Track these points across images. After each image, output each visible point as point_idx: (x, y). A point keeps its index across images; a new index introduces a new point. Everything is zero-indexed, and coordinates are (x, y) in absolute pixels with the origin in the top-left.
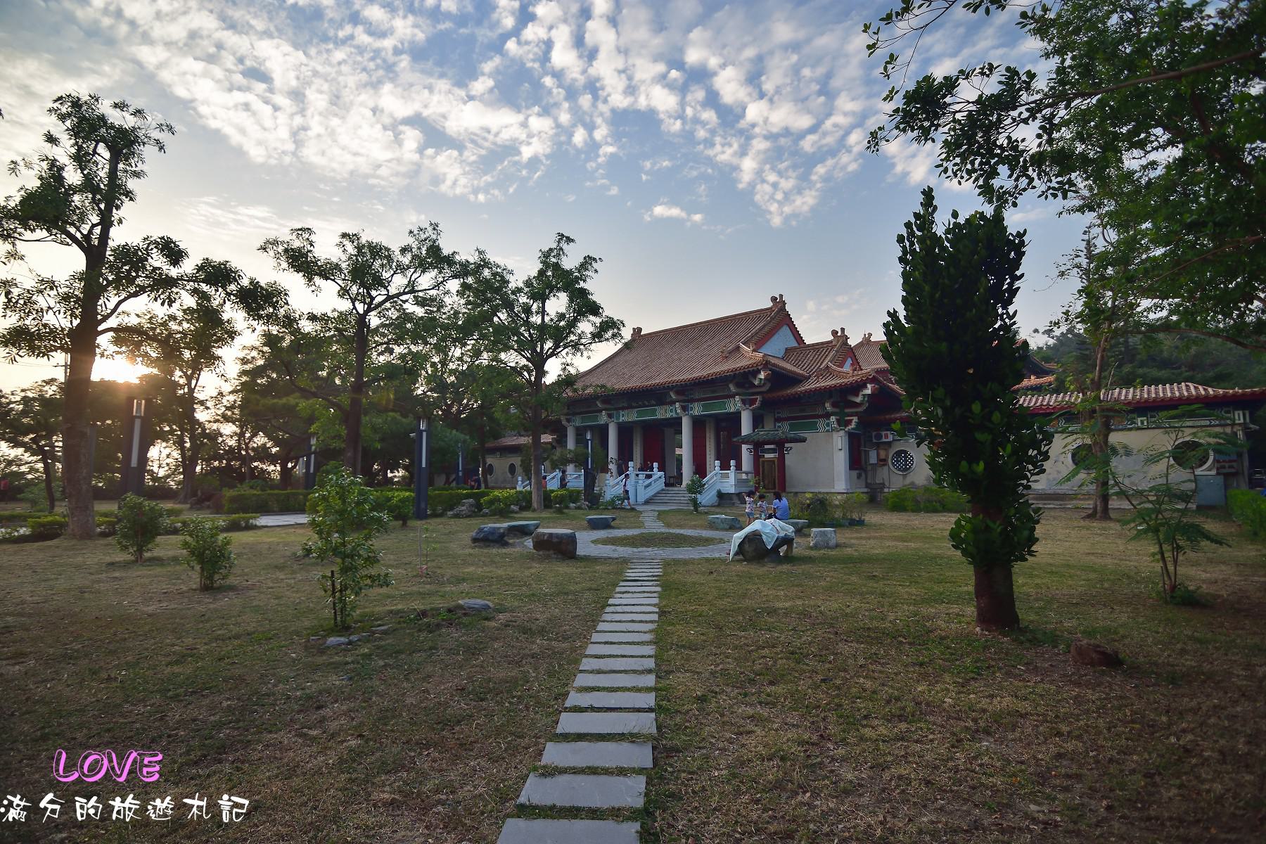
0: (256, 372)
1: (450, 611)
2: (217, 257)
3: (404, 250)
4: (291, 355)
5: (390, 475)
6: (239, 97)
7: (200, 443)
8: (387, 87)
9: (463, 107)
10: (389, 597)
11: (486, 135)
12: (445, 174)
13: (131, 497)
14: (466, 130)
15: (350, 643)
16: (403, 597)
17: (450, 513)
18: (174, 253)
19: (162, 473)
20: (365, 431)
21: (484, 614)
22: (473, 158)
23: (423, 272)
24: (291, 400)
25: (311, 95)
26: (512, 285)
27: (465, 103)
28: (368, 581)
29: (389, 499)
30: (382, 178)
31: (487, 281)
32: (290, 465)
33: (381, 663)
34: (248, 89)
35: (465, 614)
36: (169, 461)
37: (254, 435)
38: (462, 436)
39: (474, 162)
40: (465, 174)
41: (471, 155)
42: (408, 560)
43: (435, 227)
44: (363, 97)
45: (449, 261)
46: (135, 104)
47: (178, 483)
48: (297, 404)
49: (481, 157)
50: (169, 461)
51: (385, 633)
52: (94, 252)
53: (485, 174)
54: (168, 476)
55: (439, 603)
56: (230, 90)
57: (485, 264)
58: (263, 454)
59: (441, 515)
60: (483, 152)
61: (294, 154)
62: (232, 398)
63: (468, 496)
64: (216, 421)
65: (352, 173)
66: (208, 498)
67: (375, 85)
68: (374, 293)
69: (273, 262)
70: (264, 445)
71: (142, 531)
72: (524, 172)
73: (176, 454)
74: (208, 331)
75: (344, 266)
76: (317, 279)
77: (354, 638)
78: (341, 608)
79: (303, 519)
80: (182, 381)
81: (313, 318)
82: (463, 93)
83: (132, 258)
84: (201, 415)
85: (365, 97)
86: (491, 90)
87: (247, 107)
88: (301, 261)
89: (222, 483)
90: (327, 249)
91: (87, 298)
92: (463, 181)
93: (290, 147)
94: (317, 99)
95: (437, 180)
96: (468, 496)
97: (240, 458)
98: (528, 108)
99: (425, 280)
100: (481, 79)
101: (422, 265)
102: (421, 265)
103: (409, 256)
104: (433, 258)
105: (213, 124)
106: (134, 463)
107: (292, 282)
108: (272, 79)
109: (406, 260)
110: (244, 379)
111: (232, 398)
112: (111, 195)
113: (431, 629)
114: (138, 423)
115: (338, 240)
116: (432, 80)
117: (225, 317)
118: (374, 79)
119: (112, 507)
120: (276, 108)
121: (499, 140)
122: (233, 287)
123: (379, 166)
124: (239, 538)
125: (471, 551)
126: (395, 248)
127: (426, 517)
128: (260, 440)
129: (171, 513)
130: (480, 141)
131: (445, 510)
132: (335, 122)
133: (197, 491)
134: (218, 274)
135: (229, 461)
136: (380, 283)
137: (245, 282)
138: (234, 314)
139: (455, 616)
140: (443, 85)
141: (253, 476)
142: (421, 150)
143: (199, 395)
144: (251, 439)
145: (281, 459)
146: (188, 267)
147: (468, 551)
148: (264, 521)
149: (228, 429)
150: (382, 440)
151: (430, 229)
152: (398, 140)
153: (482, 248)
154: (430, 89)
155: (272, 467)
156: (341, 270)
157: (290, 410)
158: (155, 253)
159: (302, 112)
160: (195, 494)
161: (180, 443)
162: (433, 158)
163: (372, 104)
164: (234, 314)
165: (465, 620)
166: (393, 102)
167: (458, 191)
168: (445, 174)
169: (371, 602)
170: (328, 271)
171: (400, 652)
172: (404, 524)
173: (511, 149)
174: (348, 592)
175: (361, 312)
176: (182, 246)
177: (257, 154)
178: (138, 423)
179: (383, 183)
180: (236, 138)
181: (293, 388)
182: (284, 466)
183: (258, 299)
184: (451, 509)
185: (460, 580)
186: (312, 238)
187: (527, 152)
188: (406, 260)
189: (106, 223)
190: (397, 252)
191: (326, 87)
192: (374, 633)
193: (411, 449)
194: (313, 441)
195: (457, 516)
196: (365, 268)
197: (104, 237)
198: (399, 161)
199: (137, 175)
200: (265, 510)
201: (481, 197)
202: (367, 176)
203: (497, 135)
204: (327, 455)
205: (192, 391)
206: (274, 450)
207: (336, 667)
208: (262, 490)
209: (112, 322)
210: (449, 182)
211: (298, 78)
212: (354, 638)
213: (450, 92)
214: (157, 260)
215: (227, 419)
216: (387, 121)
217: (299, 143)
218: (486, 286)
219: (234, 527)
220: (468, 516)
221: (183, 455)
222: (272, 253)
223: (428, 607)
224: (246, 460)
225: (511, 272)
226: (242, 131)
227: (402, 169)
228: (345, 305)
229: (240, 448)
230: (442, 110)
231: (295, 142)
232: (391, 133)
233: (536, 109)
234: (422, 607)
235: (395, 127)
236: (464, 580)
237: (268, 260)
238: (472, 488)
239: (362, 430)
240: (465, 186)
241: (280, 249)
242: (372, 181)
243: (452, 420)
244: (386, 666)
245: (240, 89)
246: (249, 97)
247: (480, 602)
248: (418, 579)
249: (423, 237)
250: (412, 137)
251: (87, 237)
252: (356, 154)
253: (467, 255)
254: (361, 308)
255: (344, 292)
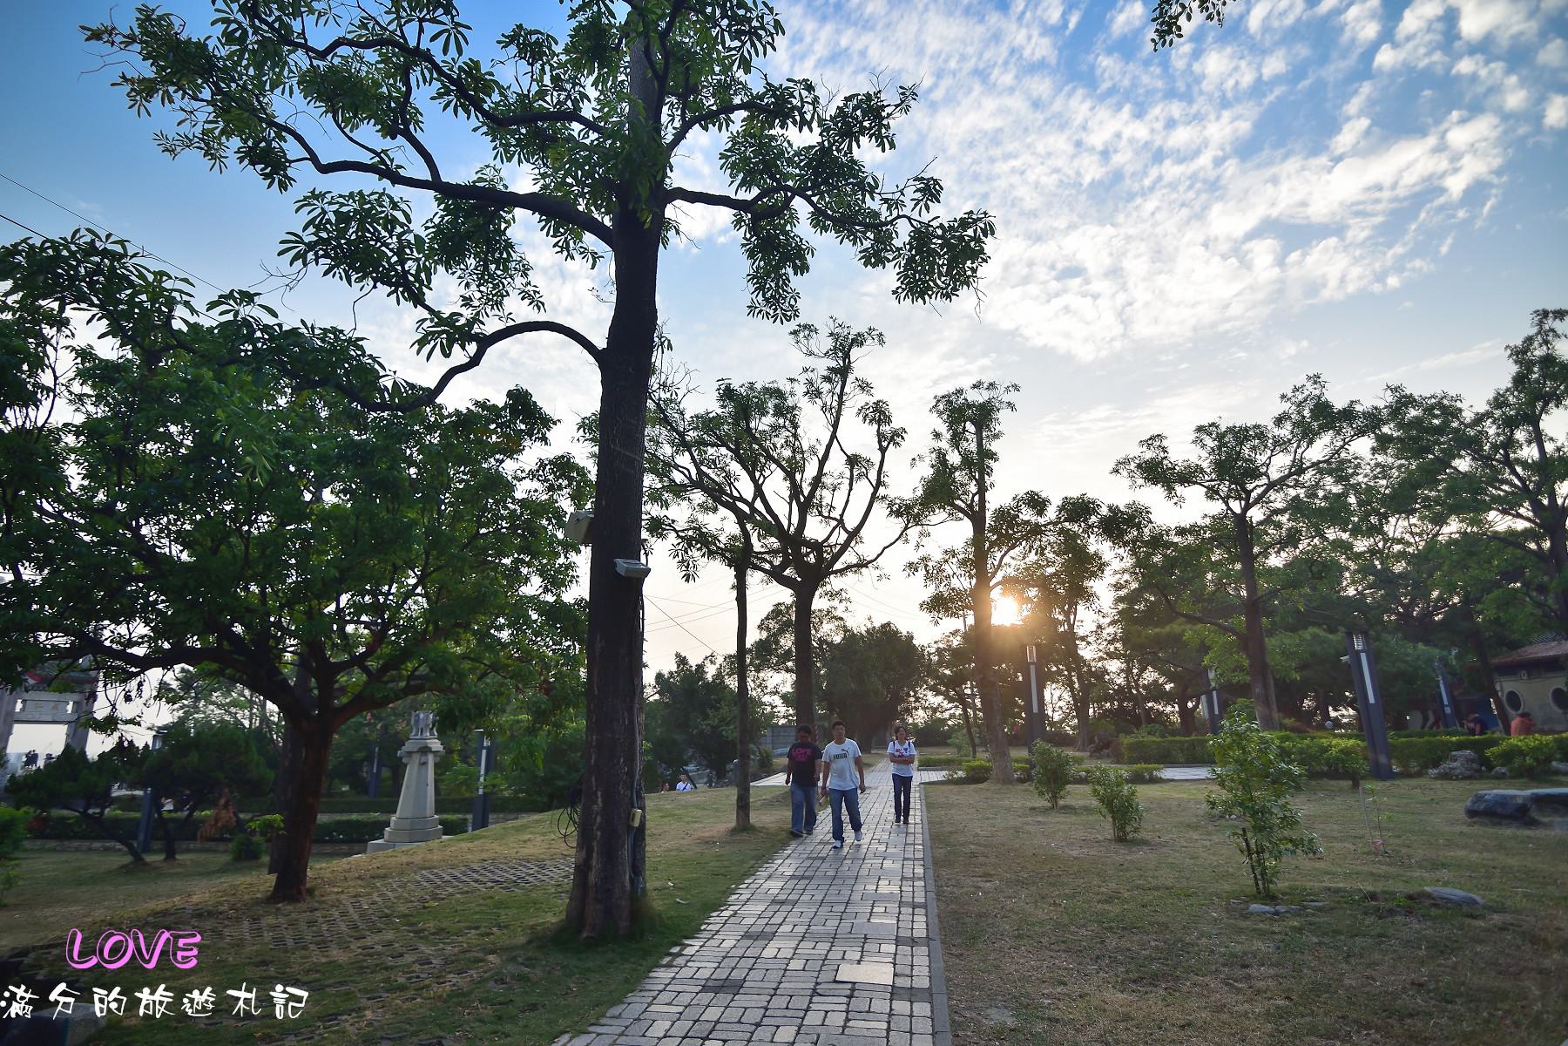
0: (1132, 598)
1: (1410, 897)
2: (1074, 494)
3: (1279, 421)
4: (1167, 568)
5: (1333, 714)
6: (1058, 303)
7: (1089, 685)
8: (1217, 208)
9: (1329, 177)
10: (1327, 873)
11: (1377, 195)
12: (1324, 276)
13: (1039, 743)
14: (1341, 204)
15: (1277, 913)
16: (1347, 876)
17: (1433, 772)
18: (1037, 502)
19: (1057, 717)
20: (1274, 659)
21: (1465, 909)
22: (1364, 234)
23: (1310, 443)
24: (1175, 627)
25: (1128, 264)
26: (1468, 416)
27: (1330, 170)
28: (1290, 846)
29: (1325, 750)
30: (1235, 319)
31: (1417, 422)
32: (1190, 705)
33: (1315, 940)
34: (1065, 291)
35: (1435, 905)
36: (1062, 704)
37: (1142, 670)
38: (1436, 652)
39: (1368, 238)
40: (1356, 261)
41: (1359, 231)
42: (1361, 832)
43: (1315, 379)
44: (1189, 235)
45: (1348, 414)
46: (987, 381)
47: (1073, 728)
48: (1182, 634)
49: (1375, 227)
50: (1062, 704)
51: (1320, 909)
52: (977, 517)
53: (1390, 246)
54: (1062, 721)
55: (1399, 887)
56: (1048, 301)
57: (1409, 401)
58: (1155, 692)
59: (1419, 774)
60: (1379, 219)
61: (1124, 336)
62: (1111, 630)
63: (1460, 746)
64: (1101, 659)
65: (1195, 329)
66: (1107, 746)
67: (1200, 216)
68: (1249, 487)
69: (1128, 482)
70: (1156, 681)
71: (1054, 779)
72: (1461, 214)
73: (1067, 696)
74: (1082, 565)
75: (1205, 465)
76: (1179, 489)
77: (1281, 908)
78: (1263, 875)
79: (1202, 773)
80: (1061, 618)
81: (1181, 532)
82: (1323, 160)
83: (1006, 517)
84: (1087, 652)
85: (1194, 234)
86: (1367, 133)
87: (1067, 309)
88: (1157, 472)
89: (1118, 724)
90: (1183, 451)
91: (977, 561)
92: (1356, 271)
93: (1119, 329)
94: (1136, 266)
95: (1313, 288)
96: (1460, 746)
97: (1132, 698)
98: (1438, 122)
99: (1318, 450)
100: (1346, 128)
101: (1307, 434)
102: (1305, 435)
103: (1288, 425)
104: (1324, 417)
105: (1039, 342)
106: (1035, 710)
107: (1152, 497)
108: (1085, 270)
109: (1285, 432)
110: (1121, 606)
111: (1111, 630)
112: (980, 463)
113: (1381, 914)
114: (1032, 668)
115: (1193, 436)
116: (1274, 170)
117: (1092, 549)
118: (1197, 208)
119: (1023, 753)
120: (1095, 297)
121: (1401, 192)
122: (1093, 519)
123: (1227, 306)
124: (1144, 792)
125: (1465, 829)
126: (1266, 421)
127: (1391, 776)
128: (1150, 676)
129: (1079, 761)
130: (1369, 208)
131: (1425, 766)
132: (1161, 280)
133: (1096, 739)
134: (1079, 509)
135: (1121, 702)
136: (1254, 473)
137: (1104, 511)
138: (1098, 545)
139: (1415, 903)
140: (1292, 164)
141: (1150, 721)
142: (1281, 262)
143: (1080, 632)
144: (1139, 675)
145: (1179, 697)
146: (1051, 513)
147: (1458, 829)
148: (1168, 773)
149: (1114, 666)
150: (1303, 667)
151: (1309, 385)
152: (1245, 263)
153: (1395, 383)
154: (1275, 181)
155: (1169, 709)
156: (1202, 471)
157: (1176, 639)
158: (1024, 508)
159: (1124, 288)
160: (1092, 741)
161: (1070, 685)
162: (1299, 263)
163: (1200, 238)
164: (1098, 545)
165: (1434, 912)
166: (1228, 222)
167: (1351, 288)
168: (1324, 276)
169: (1292, 871)
170: (1188, 476)
171: (1337, 932)
172: (1356, 785)
173: (1430, 189)
174: (1267, 855)
175: (1238, 511)
176: (1043, 495)
177: (1085, 353)
178: (1032, 668)
179: (1238, 323)
180: (1062, 345)
181: (1172, 613)
182: (1183, 707)
183: (1119, 524)
184: (1436, 765)
185: (1435, 865)
186: (1165, 443)
187: (1456, 185)
188: (1285, 432)
189: (982, 490)
190: (1271, 425)
191: (1143, 247)
192: (1305, 908)
193: (1351, 677)
194: (1211, 675)
195: (1446, 776)
196: (1233, 458)
197: (983, 501)
198: (1252, 288)
199: (996, 436)
200: (1172, 762)
201: (1393, 281)
202: (1213, 325)
203: (1394, 186)
204: (1231, 692)
205: (1071, 627)
206: (1168, 687)
207: (1262, 934)
208: (1163, 736)
209: (999, 576)
210: (1333, 283)
211: (1111, 254)
212: (1281, 908)
213: (1303, 169)
214: (1027, 514)
215: (1111, 656)
216: (1224, 247)
217: (1126, 323)
218: (1421, 430)
219: (1138, 779)
220: (1465, 778)
221: (1073, 696)
222: (1125, 473)
223: (1378, 890)
224: (1138, 700)
225: (1458, 398)
226: (1067, 336)
227: (1260, 296)
228: (1217, 507)
229: (1130, 688)
230: (1298, 197)
231: (1123, 322)
232: (1233, 260)
233: (1455, 115)
234: (1370, 888)
235: (1238, 251)
236: (1443, 865)
237: (1123, 480)
238: (1472, 732)
239: (1268, 659)
240: (1360, 278)
241: (1133, 466)
242: (1222, 328)
243: (1420, 629)
244: (1320, 944)
245: (1057, 295)
246: (1065, 299)
247: (1460, 893)
248: (1372, 857)
249: (1301, 397)
250: (1263, 252)
251: (970, 506)
252: (1193, 306)
253: (1373, 397)
254: (1236, 506)
255: (1212, 493)
